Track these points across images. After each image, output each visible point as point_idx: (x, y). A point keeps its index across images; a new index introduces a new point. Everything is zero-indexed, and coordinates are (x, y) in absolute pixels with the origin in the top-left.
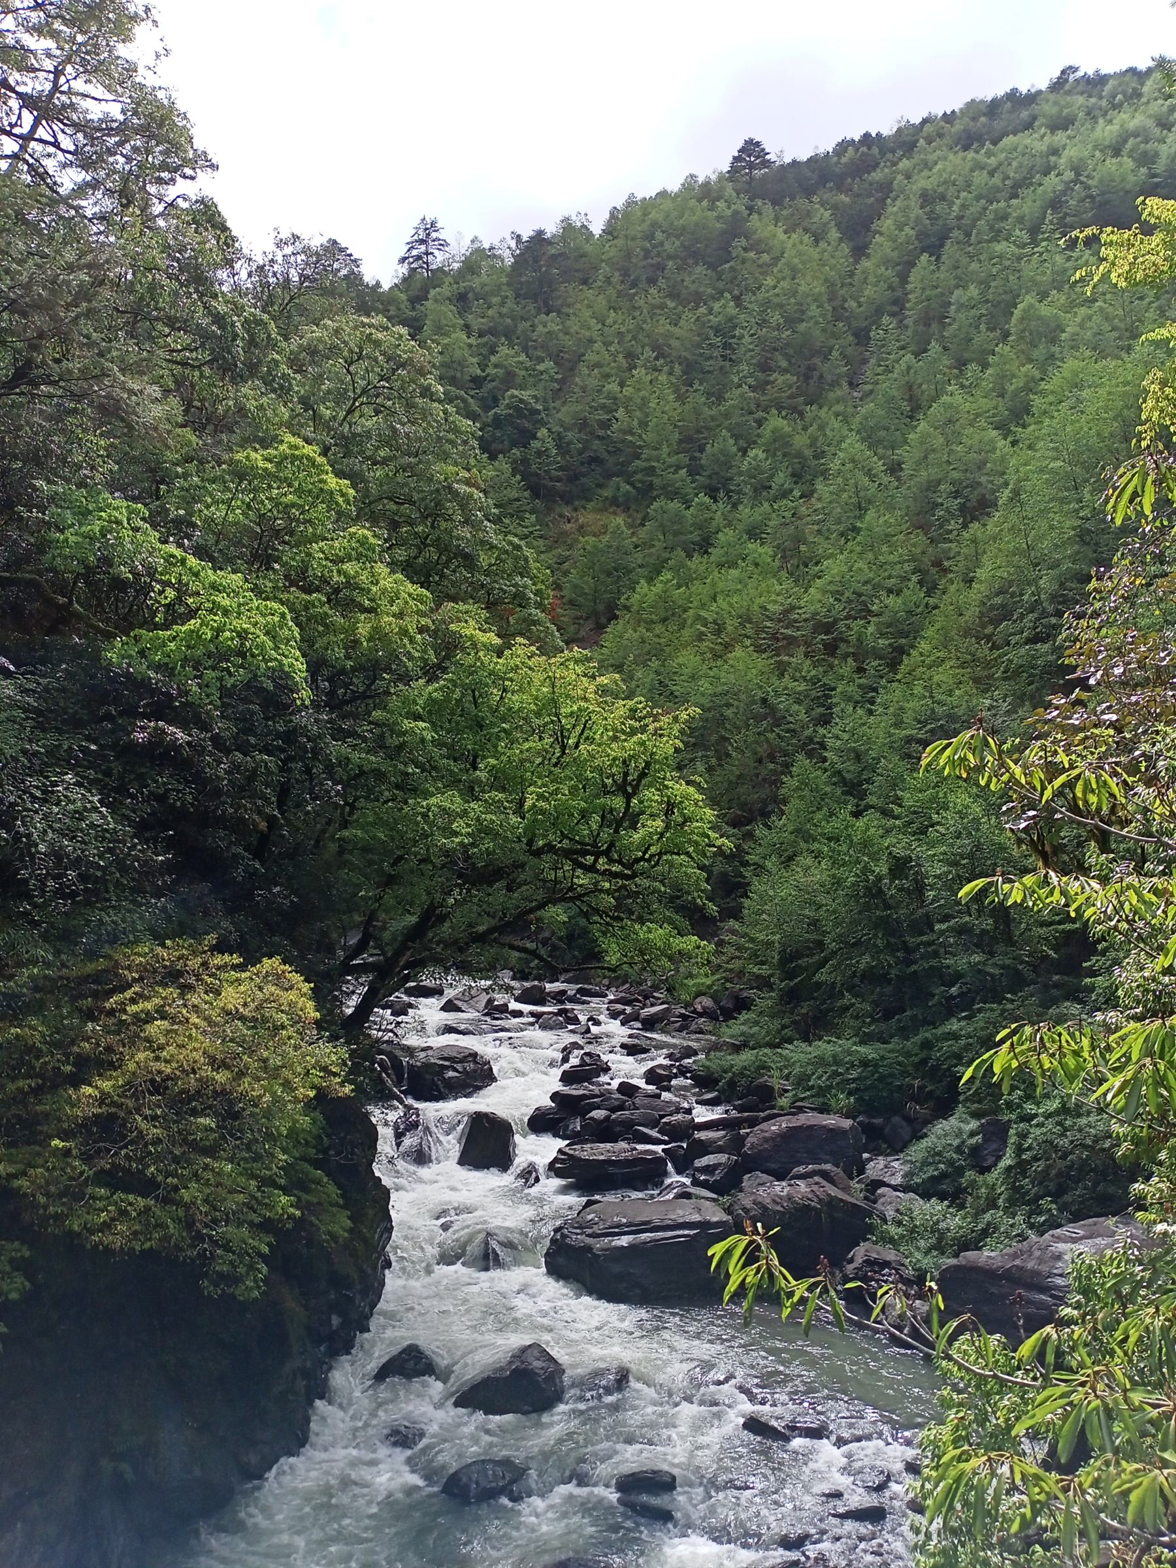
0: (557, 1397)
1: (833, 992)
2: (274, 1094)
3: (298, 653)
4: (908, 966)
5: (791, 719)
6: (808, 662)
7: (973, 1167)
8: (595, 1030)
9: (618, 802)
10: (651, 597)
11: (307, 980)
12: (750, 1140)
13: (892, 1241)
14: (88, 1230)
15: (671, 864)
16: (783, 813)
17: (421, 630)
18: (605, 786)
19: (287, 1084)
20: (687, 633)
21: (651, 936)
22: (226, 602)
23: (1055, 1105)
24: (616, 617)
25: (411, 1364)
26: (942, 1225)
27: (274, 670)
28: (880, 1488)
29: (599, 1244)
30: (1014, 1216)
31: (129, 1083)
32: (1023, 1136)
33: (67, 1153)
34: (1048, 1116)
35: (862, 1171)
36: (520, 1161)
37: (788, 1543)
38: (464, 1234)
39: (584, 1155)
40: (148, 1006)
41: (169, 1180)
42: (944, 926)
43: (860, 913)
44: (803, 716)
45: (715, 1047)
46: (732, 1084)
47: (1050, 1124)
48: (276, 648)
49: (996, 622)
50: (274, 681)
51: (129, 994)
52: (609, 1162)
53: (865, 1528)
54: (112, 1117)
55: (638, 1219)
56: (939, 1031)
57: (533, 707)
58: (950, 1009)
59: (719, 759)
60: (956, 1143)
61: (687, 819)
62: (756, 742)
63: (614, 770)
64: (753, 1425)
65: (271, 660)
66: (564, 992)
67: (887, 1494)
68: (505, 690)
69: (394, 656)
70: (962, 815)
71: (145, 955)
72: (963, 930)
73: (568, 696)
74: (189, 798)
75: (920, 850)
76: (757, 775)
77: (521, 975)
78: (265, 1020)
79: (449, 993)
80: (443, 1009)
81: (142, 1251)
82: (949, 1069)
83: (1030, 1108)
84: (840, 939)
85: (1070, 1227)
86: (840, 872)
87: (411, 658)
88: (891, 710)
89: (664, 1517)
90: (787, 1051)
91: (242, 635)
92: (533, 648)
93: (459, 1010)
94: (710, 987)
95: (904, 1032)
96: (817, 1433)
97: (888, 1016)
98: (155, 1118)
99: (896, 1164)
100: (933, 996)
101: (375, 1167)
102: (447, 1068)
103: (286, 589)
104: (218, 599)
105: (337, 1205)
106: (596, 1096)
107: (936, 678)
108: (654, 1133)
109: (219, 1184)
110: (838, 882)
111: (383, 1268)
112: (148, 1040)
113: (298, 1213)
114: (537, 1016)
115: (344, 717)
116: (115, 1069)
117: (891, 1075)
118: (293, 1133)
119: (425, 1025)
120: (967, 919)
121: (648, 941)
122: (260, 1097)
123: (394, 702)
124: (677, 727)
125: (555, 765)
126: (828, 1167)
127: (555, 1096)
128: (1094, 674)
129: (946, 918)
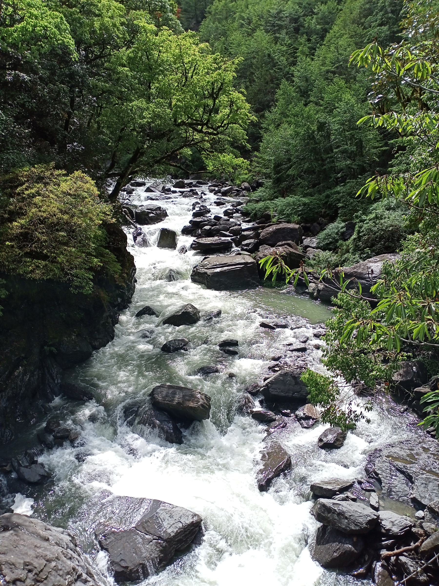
0: (198, 319)
1: (293, 178)
2: (86, 223)
3: (70, 36)
4: (322, 167)
5: (279, 63)
6: (287, 37)
7: (342, 239)
8: (204, 197)
9: (210, 102)
10: (220, 7)
11: (93, 179)
12: (262, 234)
13: (311, 265)
14: (26, 273)
15: (232, 128)
16: (276, 106)
17: (122, 24)
18: (204, 94)
19: (91, 219)
20: (236, 24)
21: (225, 159)
22: (36, 12)
23: (373, 216)
24: (205, 17)
25: (148, 311)
26: (329, 259)
27: (61, 44)
28: (305, 342)
29: (209, 272)
30: (355, 255)
31: (31, 220)
32: (361, 227)
33: (12, 246)
34: (370, 220)
35: (302, 242)
36: (180, 245)
37: (274, 359)
38: (162, 269)
39: (202, 242)
40: (33, 191)
41: (52, 255)
42: (337, 150)
43: (305, 146)
44: (285, 62)
45: (249, 201)
46: (255, 214)
47: (371, 223)
48: (61, 34)
49: (366, 17)
50: (61, 50)
51: (24, 187)
52: (212, 244)
53: (300, 354)
54: (27, 233)
55: (223, 263)
56: (333, 191)
57: (172, 59)
58: (337, 182)
59: (250, 83)
60: (336, 231)
61: (239, 108)
62: (266, 74)
63: (208, 87)
64: (263, 325)
65: (59, 40)
66: (192, 183)
67: (307, 343)
68: (160, 52)
69: (111, 37)
70: (347, 104)
71: (28, 171)
72: (344, 152)
73: (187, 53)
74: (34, 105)
75: (330, 119)
76: (266, 89)
77: (175, 177)
78: (79, 196)
79: (148, 185)
80: (146, 191)
81: (47, 279)
82: (335, 205)
83: (364, 217)
84: (297, 157)
85: (375, 258)
86: (299, 130)
87: (118, 38)
88: (321, 58)
89: (234, 353)
90: (276, 201)
91: (45, 28)
92: (171, 31)
93: (152, 191)
94: (247, 179)
95: (320, 192)
96: (285, 327)
97: (314, 186)
98: (43, 233)
99: (314, 240)
100: (331, 178)
101: (127, 248)
102: (150, 213)
103: (61, 7)
104: (32, 11)
105: (115, 261)
106: (206, 221)
107: (340, 43)
108: (227, 233)
109: (71, 255)
110: (297, 134)
111: (134, 282)
112: (35, 204)
113: (102, 264)
114: (182, 192)
115: (93, 66)
116: (25, 215)
117: (314, 208)
118: (96, 237)
119: (140, 198)
120: (346, 147)
121: (223, 161)
122: (81, 224)
123: (113, 59)
124: (234, 66)
125: (183, 86)
126: (289, 242)
127: (190, 222)
128: (411, 32)
129: (338, 147)
